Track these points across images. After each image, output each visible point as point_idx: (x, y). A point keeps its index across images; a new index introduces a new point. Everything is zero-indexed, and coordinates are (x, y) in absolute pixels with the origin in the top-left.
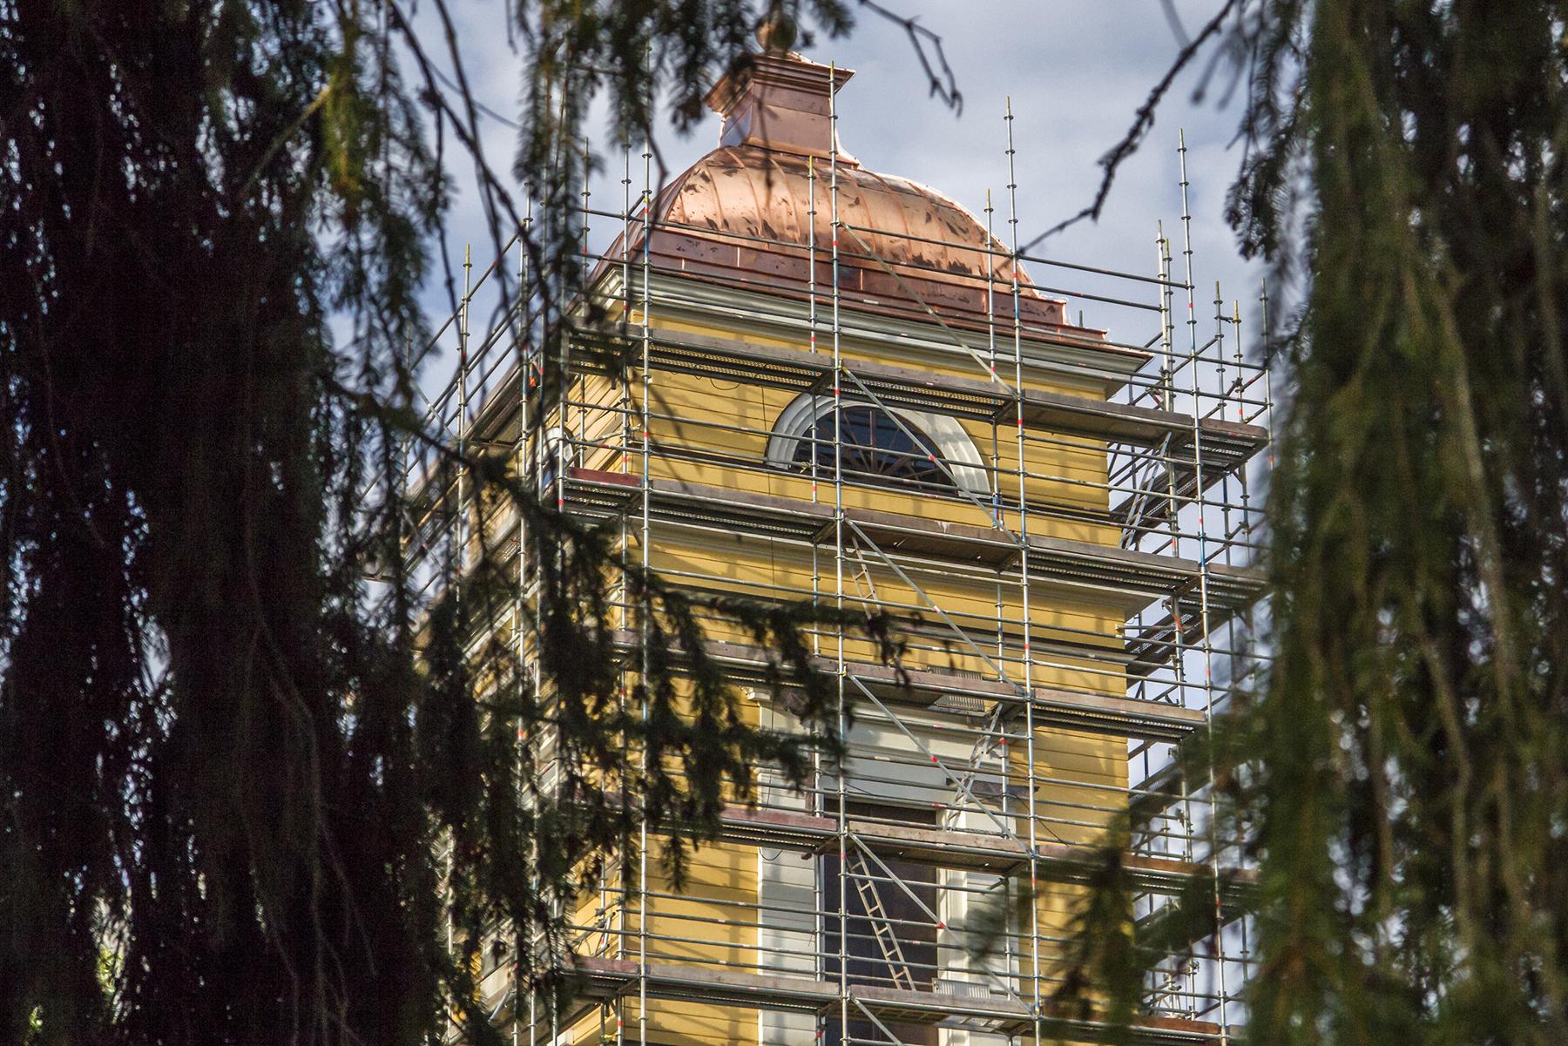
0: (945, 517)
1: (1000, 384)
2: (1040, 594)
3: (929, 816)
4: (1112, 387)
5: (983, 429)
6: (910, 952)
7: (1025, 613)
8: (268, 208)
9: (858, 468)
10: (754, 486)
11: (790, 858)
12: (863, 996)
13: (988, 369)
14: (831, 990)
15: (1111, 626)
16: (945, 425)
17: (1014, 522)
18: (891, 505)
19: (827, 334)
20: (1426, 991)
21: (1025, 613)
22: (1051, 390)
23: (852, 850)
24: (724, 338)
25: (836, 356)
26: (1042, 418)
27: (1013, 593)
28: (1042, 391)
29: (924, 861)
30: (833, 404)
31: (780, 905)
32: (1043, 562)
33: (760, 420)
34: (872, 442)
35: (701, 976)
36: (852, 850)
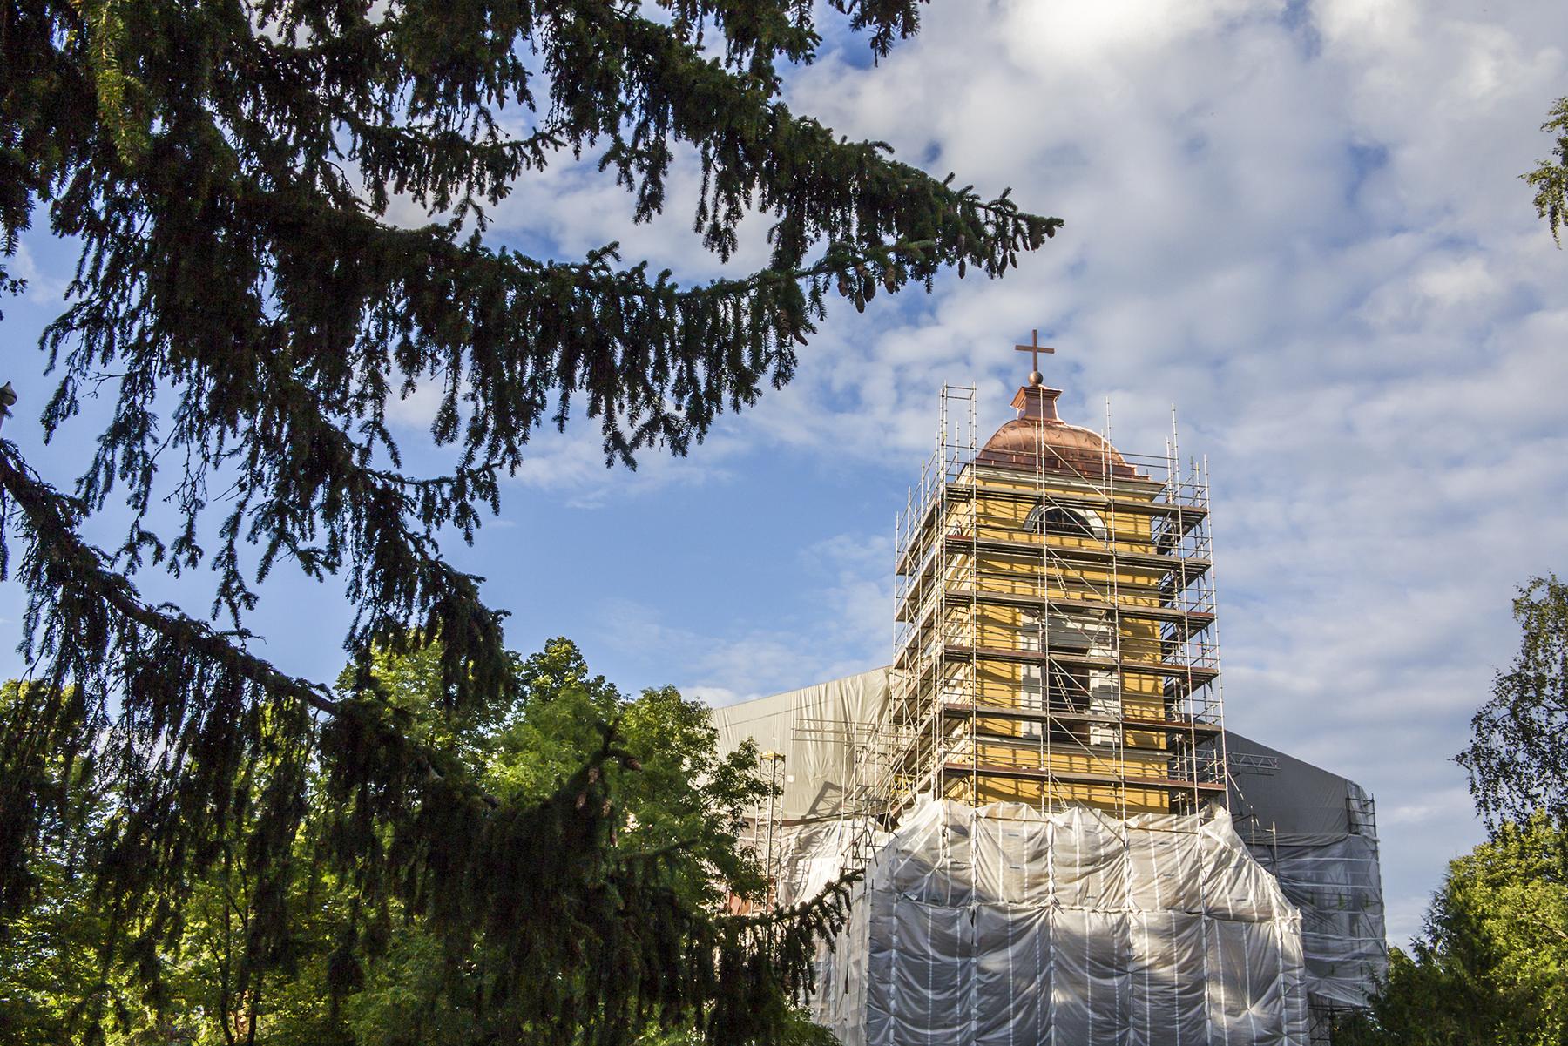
0: (1090, 546)
1: (1105, 498)
2: (1120, 571)
3: (1084, 651)
4: (1152, 498)
5: (1102, 514)
6: (1074, 700)
7: (1115, 578)
8: (264, 126)
9: (1052, 530)
10: (1020, 539)
11: (1033, 668)
12: (1055, 715)
13: (1102, 492)
14: (1043, 714)
15: (1154, 581)
16: (1090, 513)
17: (1113, 546)
18: (1071, 543)
19: (1039, 483)
20: (152, 329)
21: (1115, 578)
22: (1423, 810)
23: (1051, 664)
24: (1008, 488)
25: (1043, 491)
26: (1120, 508)
27: (1111, 571)
28: (1120, 499)
29: (1085, 668)
30: (1044, 509)
31: (1029, 684)
32: (1120, 560)
33: (1022, 515)
34: (1062, 520)
35: (996, 710)
36: (1051, 664)
